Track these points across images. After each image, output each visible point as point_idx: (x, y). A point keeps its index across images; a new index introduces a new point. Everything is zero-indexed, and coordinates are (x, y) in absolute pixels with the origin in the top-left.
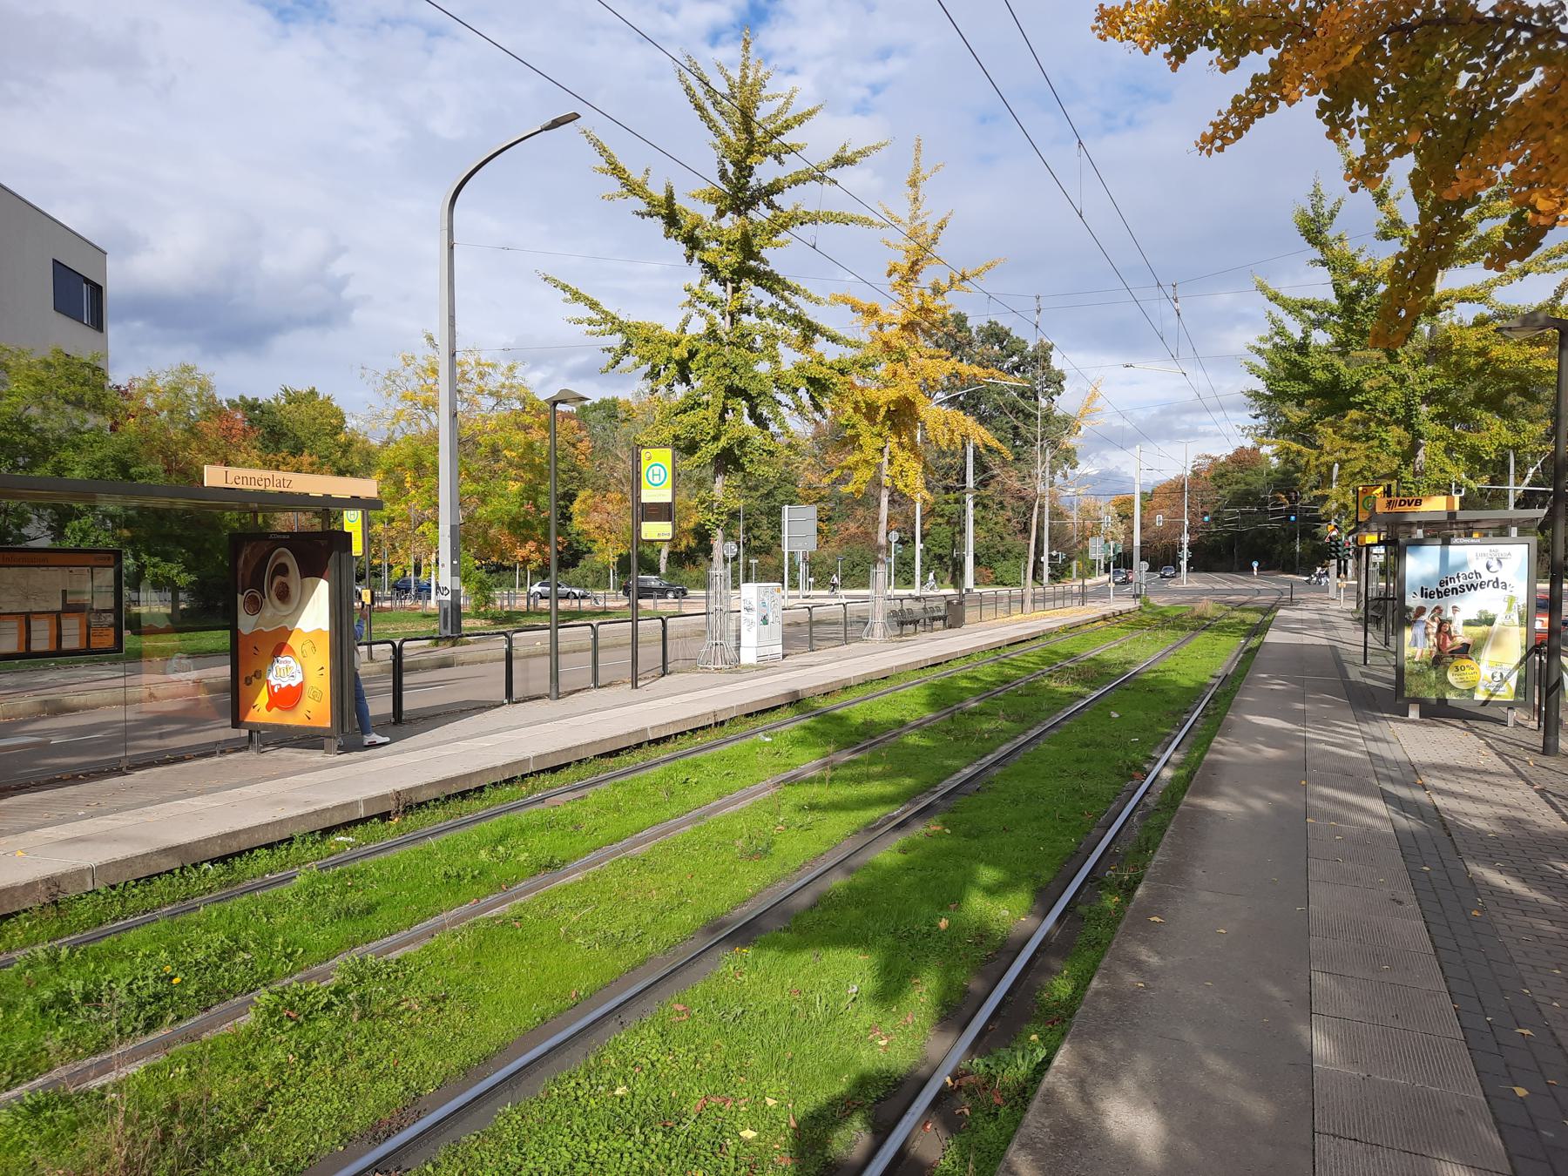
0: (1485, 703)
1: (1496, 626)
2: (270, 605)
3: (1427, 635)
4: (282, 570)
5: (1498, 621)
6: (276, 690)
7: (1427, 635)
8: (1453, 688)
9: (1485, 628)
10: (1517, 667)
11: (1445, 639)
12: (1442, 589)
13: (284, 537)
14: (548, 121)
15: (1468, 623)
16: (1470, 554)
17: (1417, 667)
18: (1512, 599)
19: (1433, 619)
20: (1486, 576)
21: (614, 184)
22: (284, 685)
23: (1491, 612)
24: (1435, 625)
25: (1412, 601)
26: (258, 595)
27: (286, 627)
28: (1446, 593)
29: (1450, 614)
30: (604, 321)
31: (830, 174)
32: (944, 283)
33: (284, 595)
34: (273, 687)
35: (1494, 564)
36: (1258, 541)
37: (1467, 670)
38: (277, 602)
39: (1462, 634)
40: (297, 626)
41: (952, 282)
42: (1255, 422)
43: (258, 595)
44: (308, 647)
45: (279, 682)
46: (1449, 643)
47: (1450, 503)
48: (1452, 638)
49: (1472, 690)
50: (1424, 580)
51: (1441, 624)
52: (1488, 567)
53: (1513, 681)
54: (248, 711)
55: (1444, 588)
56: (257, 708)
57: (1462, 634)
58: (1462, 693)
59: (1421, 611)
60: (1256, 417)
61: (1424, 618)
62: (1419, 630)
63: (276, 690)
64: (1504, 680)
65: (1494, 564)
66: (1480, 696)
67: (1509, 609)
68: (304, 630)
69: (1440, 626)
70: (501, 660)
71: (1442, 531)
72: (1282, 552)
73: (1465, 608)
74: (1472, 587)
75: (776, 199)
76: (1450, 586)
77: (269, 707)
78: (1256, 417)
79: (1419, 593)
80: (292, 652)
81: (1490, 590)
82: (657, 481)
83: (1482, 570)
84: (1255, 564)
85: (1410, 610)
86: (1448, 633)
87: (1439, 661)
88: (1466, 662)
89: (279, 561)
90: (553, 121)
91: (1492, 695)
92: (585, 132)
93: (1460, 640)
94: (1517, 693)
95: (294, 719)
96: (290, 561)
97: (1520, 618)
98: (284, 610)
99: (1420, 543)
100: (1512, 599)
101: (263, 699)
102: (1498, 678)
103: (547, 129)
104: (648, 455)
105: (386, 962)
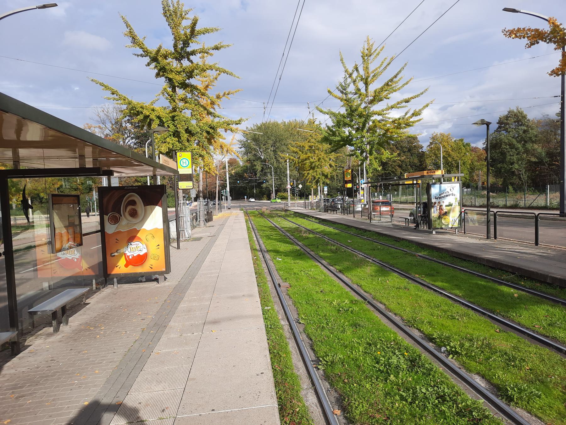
0: (452, 228)
1: (453, 206)
2: (124, 218)
3: (437, 210)
4: (133, 203)
5: (453, 205)
6: (130, 257)
7: (437, 210)
8: (444, 224)
9: (450, 207)
10: (458, 217)
11: (441, 211)
12: (440, 197)
13: (134, 188)
14: (41, 4)
15: (446, 206)
16: (446, 186)
17: (435, 219)
18: (456, 199)
19: (438, 205)
20: (450, 193)
21: (129, 40)
22: (135, 255)
23: (451, 203)
24: (439, 207)
25: (433, 200)
26: (117, 215)
27: (136, 229)
28: (441, 198)
29: (442, 204)
30: (120, 99)
31: (211, 51)
32: (221, 94)
33: (134, 214)
34: (128, 257)
35: (452, 189)
36: (241, 189)
37: (447, 219)
38: (130, 218)
39: (445, 209)
40: (143, 227)
41: (224, 94)
42: (241, 150)
43: (117, 215)
44: (149, 237)
45: (132, 254)
46: (442, 212)
47: (442, 172)
48: (443, 210)
49: (448, 225)
50: (436, 194)
51: (440, 206)
52: (451, 190)
53: (457, 221)
54: (113, 269)
55: (440, 197)
56: (118, 267)
57: (445, 209)
58: (446, 225)
59: (435, 203)
60: (241, 148)
61: (436, 205)
62: (435, 209)
63: (130, 257)
64: (455, 221)
65: (452, 189)
66: (450, 226)
67: (456, 201)
68: (147, 229)
69: (440, 207)
70: (17, 251)
71: (439, 181)
72: (250, 193)
73: (446, 201)
74: (447, 196)
75: (192, 57)
76: (442, 196)
77: (126, 266)
78: (241, 148)
79: (434, 198)
80: (140, 240)
81: (451, 196)
82: (184, 165)
83: (449, 191)
84: (246, 197)
85: (432, 203)
86: (442, 209)
87: (440, 217)
88: (447, 217)
89: (130, 199)
90: (44, 5)
91: (453, 226)
92: (122, 17)
93: (445, 211)
94: (458, 224)
95: (144, 269)
96: (137, 198)
97: (458, 204)
98: (134, 220)
99: (435, 184)
100: (456, 199)
101: (122, 262)
102: (454, 221)
103: (39, 8)
104: (181, 155)
105: (454, 326)
